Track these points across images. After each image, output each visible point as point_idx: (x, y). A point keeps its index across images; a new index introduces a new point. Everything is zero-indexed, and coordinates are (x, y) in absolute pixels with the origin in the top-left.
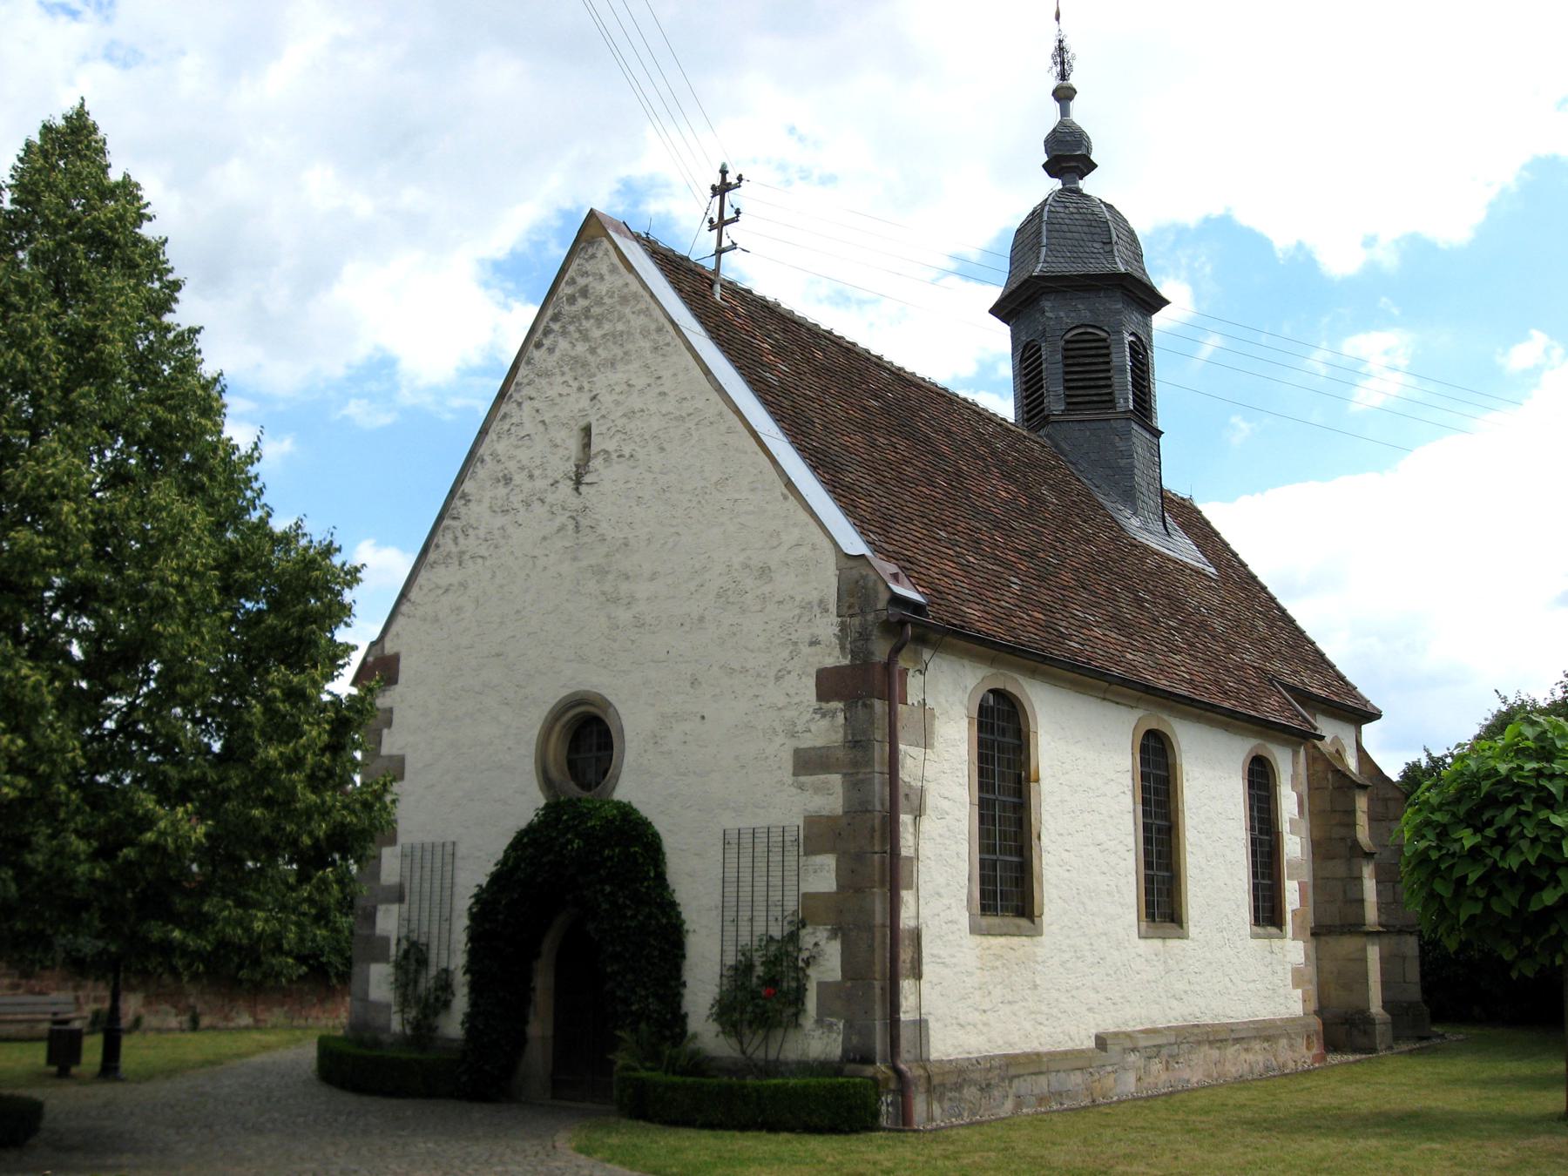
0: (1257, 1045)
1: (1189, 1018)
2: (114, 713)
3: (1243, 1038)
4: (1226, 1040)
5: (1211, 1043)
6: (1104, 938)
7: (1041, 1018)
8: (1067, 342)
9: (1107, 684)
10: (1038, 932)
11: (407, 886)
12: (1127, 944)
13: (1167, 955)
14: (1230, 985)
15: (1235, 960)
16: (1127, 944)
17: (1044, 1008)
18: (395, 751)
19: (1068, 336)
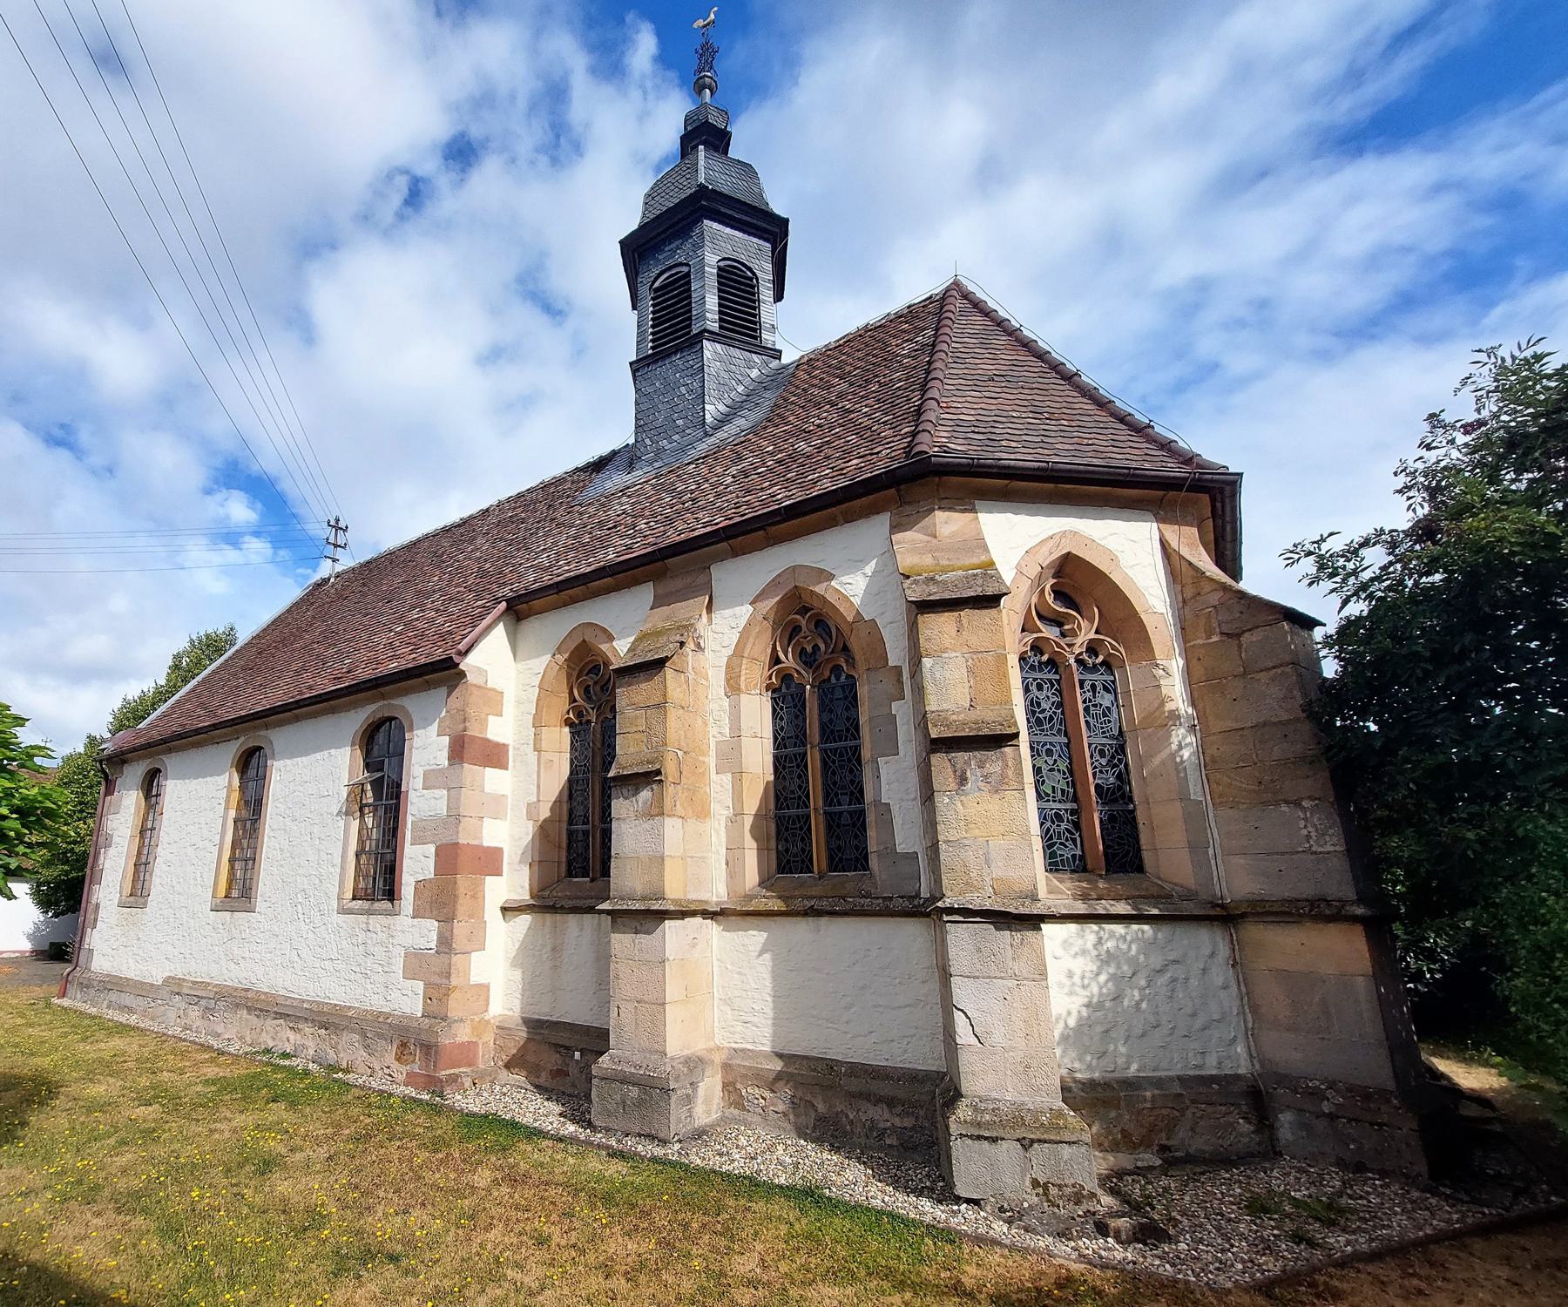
0: (307, 1029)
1: (244, 982)
2: (1429, 816)
3: (288, 1015)
4: (267, 1011)
5: (249, 1009)
6: (184, 910)
7: (139, 958)
8: (656, 290)
9: (761, 533)
10: (144, 906)
11: (214, 531)
12: (200, 915)
13: (232, 925)
14: (296, 958)
15: (311, 935)
16: (200, 915)
17: (141, 953)
18: (464, 669)
19: (657, 285)
